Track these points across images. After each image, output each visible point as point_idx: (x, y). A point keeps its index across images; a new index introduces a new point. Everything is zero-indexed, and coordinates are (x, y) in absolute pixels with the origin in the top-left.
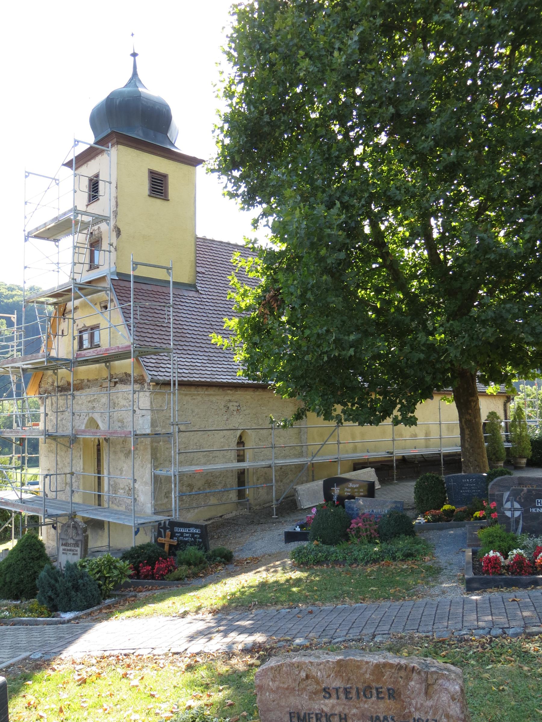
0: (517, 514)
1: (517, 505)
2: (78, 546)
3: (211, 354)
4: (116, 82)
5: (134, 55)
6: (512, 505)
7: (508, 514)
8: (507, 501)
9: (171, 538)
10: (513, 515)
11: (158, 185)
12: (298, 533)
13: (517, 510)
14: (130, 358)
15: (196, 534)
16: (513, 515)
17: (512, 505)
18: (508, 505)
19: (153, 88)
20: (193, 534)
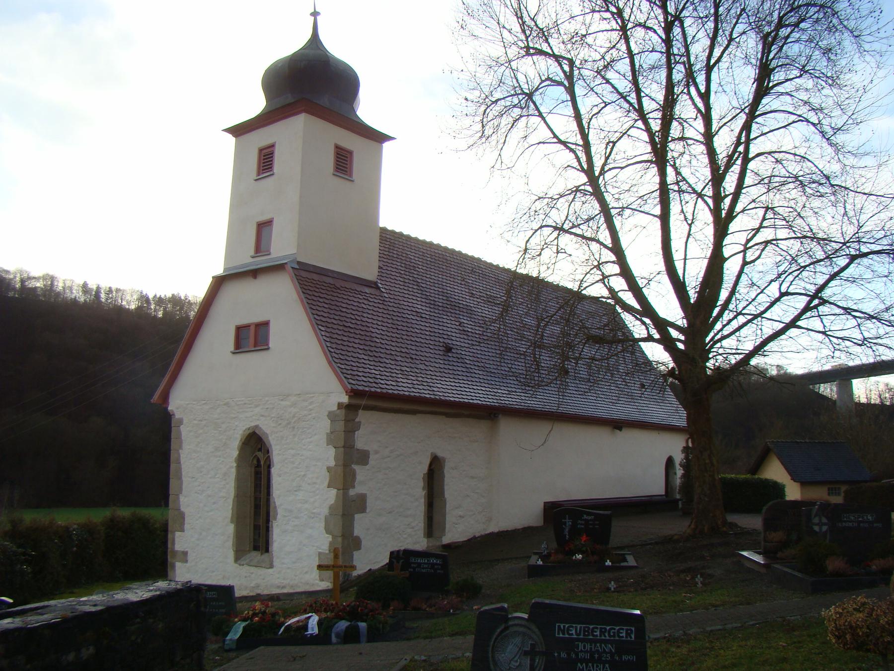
0: (825, 528)
1: (824, 520)
2: (839, 488)
3: (334, 331)
4: (291, 43)
5: (315, 14)
6: (820, 520)
7: (816, 528)
8: (815, 516)
9: (401, 570)
10: (821, 529)
11: (343, 162)
12: (540, 565)
13: (825, 524)
14: (839, 494)
15: (436, 564)
16: (821, 529)
17: (820, 520)
18: (816, 520)
19: (338, 47)
20: (433, 565)
